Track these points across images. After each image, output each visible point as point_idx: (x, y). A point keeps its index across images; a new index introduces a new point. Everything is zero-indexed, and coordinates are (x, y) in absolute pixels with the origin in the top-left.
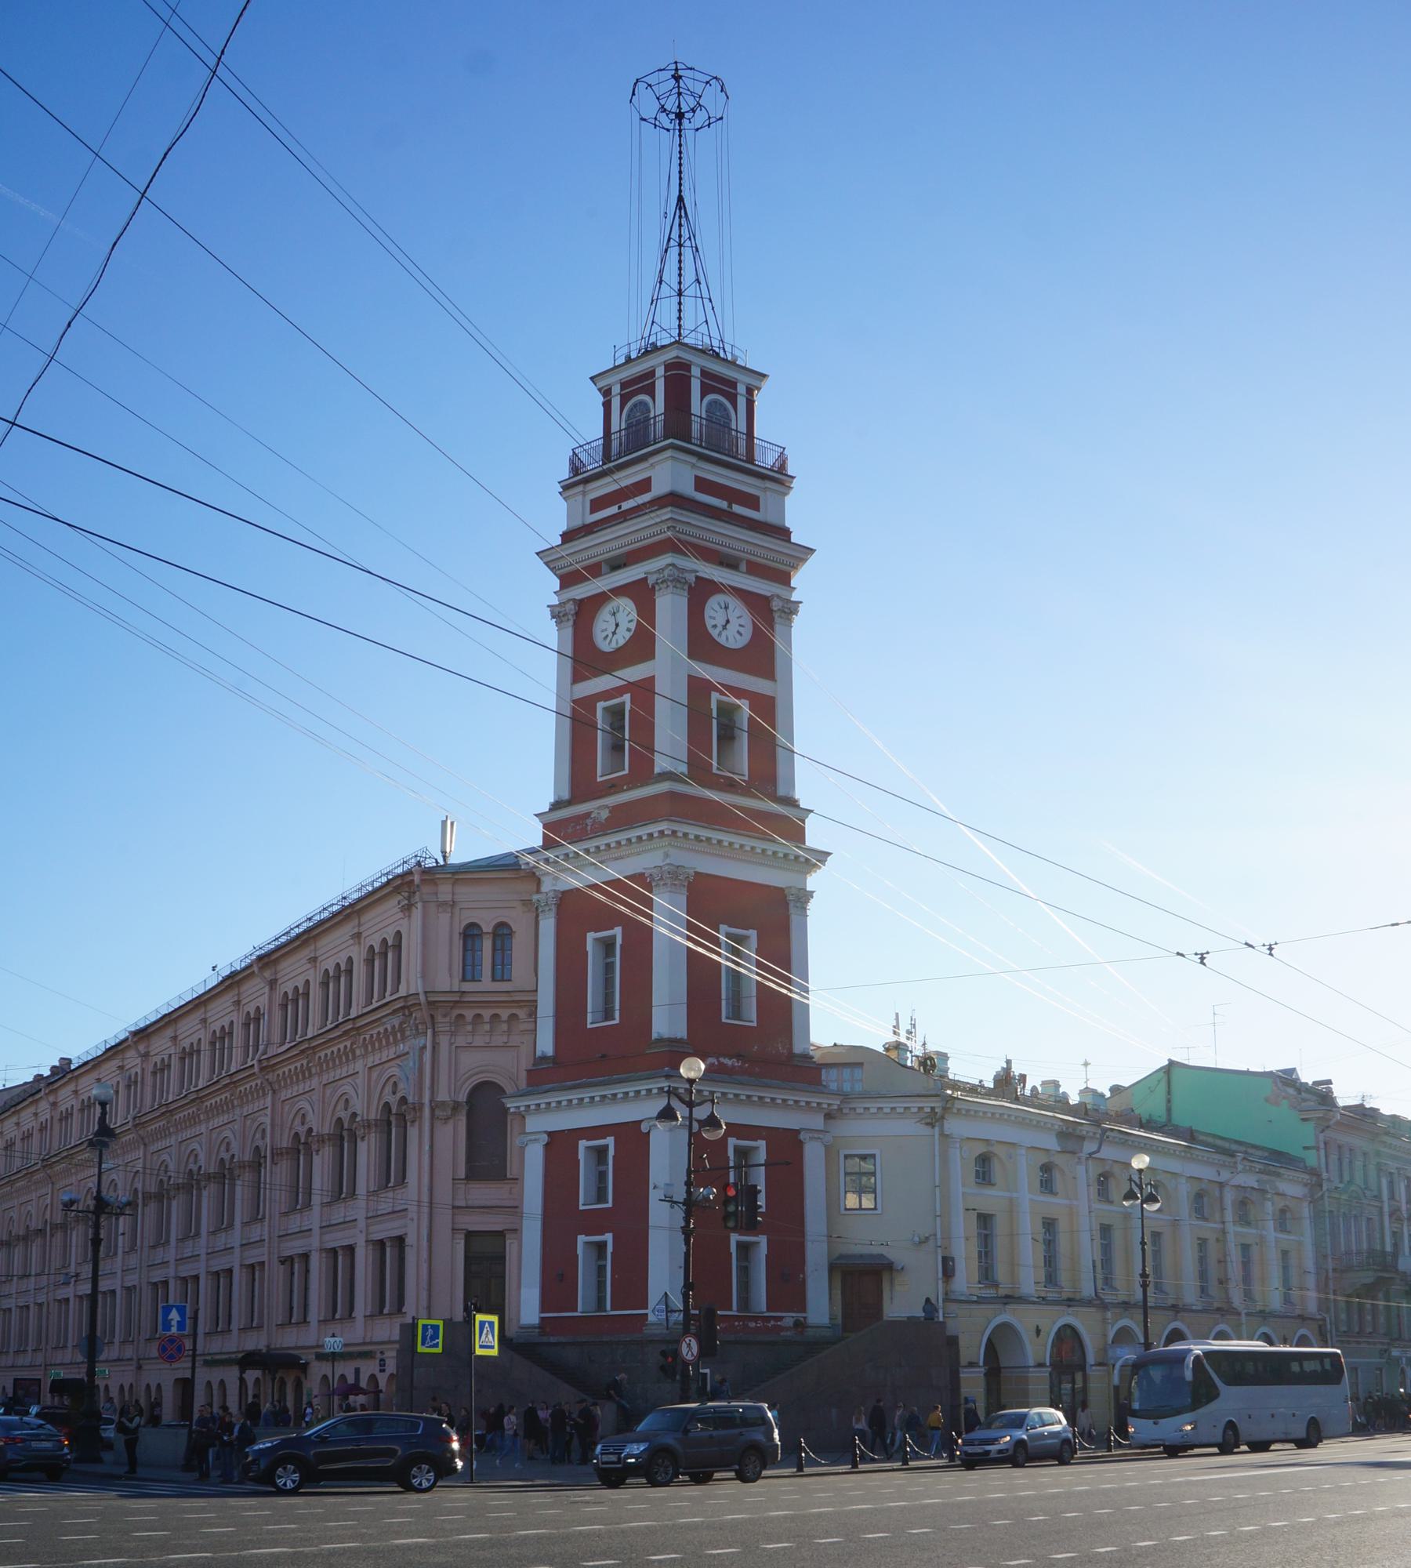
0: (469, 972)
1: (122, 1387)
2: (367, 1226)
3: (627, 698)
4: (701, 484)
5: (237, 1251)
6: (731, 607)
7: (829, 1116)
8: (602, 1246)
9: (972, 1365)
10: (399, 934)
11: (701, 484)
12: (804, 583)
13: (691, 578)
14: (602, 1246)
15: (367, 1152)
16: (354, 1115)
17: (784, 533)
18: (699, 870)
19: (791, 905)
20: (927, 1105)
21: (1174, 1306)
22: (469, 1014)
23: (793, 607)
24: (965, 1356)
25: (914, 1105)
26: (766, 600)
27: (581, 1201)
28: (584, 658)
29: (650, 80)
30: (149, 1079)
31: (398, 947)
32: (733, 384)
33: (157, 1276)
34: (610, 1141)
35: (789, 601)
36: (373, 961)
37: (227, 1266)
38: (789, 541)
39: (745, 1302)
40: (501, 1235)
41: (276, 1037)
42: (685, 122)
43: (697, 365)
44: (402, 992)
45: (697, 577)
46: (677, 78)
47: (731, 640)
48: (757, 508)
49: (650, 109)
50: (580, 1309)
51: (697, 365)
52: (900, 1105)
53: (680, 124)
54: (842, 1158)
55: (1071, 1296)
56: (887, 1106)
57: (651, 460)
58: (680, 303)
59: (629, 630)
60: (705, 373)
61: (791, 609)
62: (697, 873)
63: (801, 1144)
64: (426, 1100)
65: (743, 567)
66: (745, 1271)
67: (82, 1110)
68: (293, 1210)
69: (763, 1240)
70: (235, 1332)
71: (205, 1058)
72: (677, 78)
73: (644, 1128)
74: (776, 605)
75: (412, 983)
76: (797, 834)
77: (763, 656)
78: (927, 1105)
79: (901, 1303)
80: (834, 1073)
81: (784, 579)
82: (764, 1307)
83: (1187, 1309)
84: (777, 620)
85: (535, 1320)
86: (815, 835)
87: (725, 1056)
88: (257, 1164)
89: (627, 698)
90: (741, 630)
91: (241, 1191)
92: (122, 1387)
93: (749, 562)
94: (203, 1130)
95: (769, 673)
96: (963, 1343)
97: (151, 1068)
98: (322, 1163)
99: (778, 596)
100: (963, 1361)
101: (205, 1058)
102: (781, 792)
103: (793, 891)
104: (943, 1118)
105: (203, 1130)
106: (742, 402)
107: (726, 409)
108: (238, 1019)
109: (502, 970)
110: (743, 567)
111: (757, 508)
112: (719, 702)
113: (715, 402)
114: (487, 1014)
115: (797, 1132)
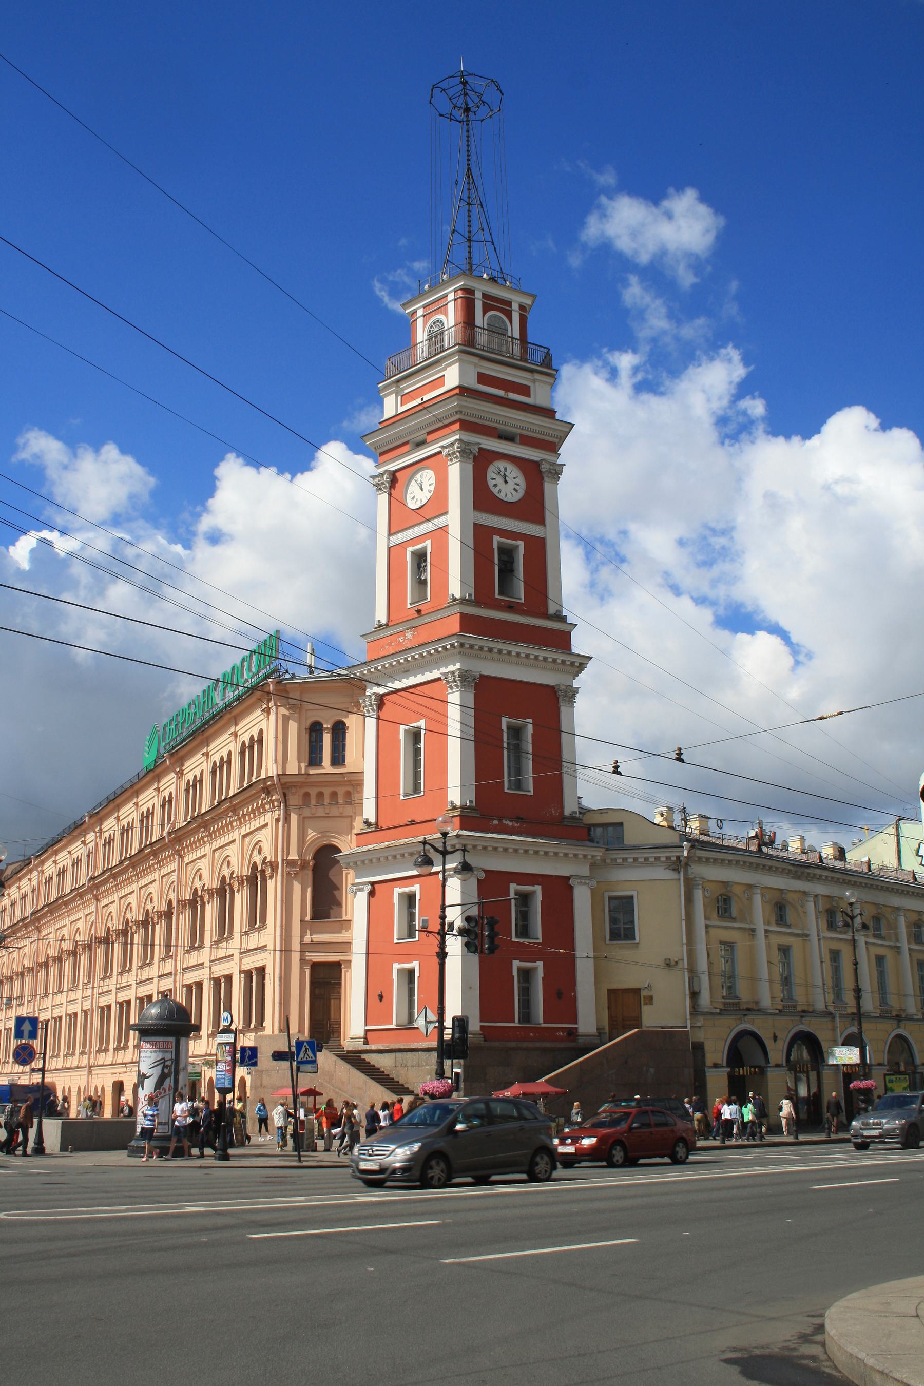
0: (314, 759)
1: (79, 1088)
2: (241, 959)
3: (428, 543)
4: (483, 378)
5: (156, 980)
6: (509, 471)
7: (593, 865)
8: (411, 972)
9: (716, 1066)
10: (261, 732)
11: (483, 378)
12: (567, 452)
13: (475, 450)
14: (411, 972)
15: (241, 900)
16: (233, 873)
17: (550, 413)
18: (483, 673)
19: (561, 699)
20: (673, 854)
21: (897, 1016)
22: (313, 792)
23: (558, 468)
24: (710, 1059)
25: (663, 855)
26: (537, 464)
27: (396, 936)
28: (481, 497)
29: (444, 85)
30: (101, 849)
31: (260, 741)
32: (509, 304)
33: (103, 1002)
34: (521, 544)
35: (554, 464)
36: (245, 752)
37: (148, 993)
38: (554, 418)
39: (526, 1016)
40: (338, 965)
41: (182, 818)
42: (471, 115)
43: (479, 290)
44: (263, 776)
45: (480, 449)
46: (465, 83)
47: (509, 495)
48: (528, 394)
49: (446, 108)
50: (517, 1019)
51: (479, 290)
52: (651, 855)
53: (467, 116)
54: (607, 900)
55: (806, 1008)
56: (641, 856)
57: (537, 376)
58: (470, 247)
59: (430, 491)
60: (485, 296)
61: (556, 472)
62: (481, 676)
63: (571, 888)
64: (280, 860)
65: (518, 439)
66: (526, 992)
67: (59, 875)
68: (193, 948)
69: (540, 965)
70: (131, 1047)
71: (136, 832)
72: (465, 83)
73: (571, 882)
74: (544, 467)
75: (270, 769)
76: (562, 640)
77: (534, 505)
78: (673, 854)
79: (653, 1018)
80: (599, 830)
81: (553, 447)
82: (541, 1020)
83: (909, 1018)
84: (546, 479)
85: (478, 1028)
86: (580, 644)
87: (507, 818)
88: (168, 914)
89: (428, 543)
90: (517, 487)
91: (159, 931)
92: (79, 1088)
93: (521, 435)
94: (135, 888)
95: (540, 519)
96: (708, 1047)
97: (102, 842)
98: (211, 910)
99: (545, 460)
100: (709, 1062)
101: (136, 832)
102: (552, 610)
103: (562, 687)
104: (687, 865)
105: (135, 888)
106: (516, 317)
107: (503, 322)
108: (158, 802)
109: (338, 758)
110: (518, 439)
111: (528, 394)
112: (499, 542)
113: (495, 316)
114: (327, 791)
115: (568, 878)
